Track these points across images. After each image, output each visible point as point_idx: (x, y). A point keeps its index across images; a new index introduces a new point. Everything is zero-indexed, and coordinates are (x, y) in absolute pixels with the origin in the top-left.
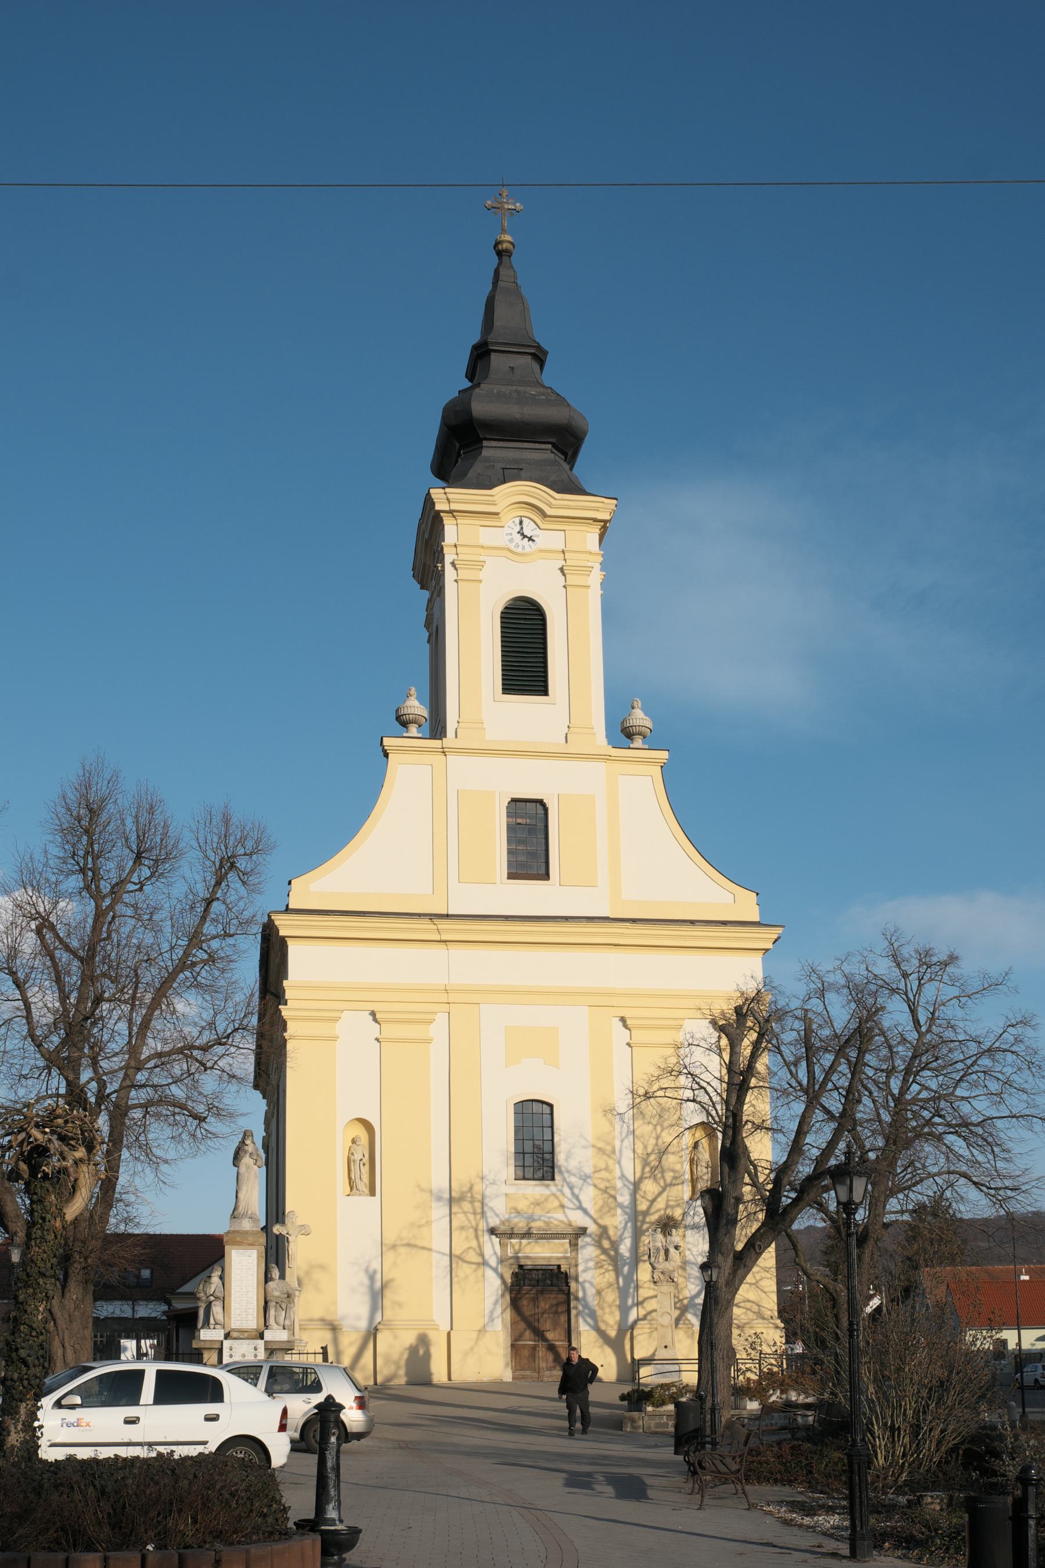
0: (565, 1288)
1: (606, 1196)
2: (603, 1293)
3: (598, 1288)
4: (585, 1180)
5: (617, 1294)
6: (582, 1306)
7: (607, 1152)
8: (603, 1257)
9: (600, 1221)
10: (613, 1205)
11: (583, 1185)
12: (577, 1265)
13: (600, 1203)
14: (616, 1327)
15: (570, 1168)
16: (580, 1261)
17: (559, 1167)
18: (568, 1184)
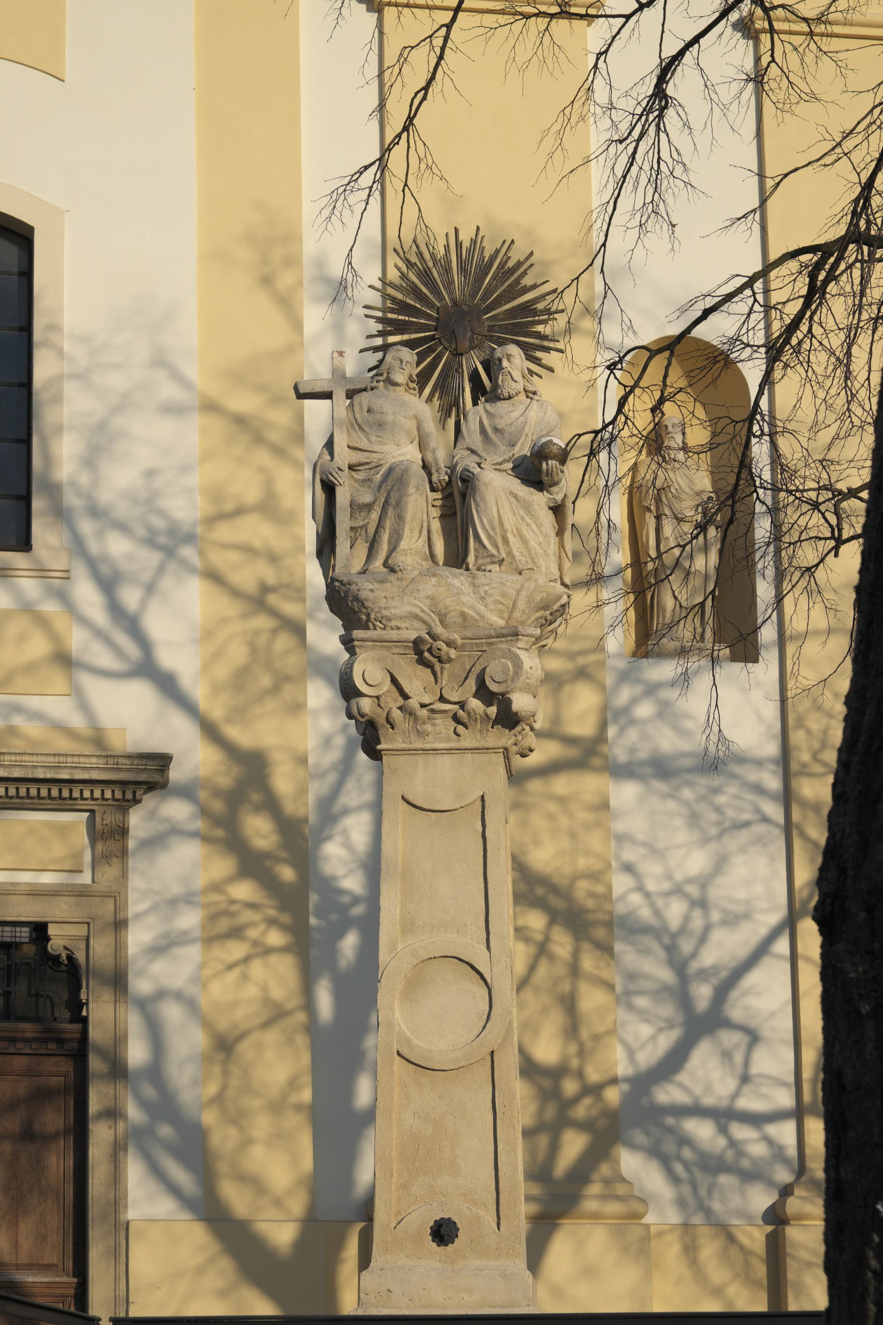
0: (71, 1029)
1: (263, 622)
2: (245, 1047)
3: (223, 1024)
4: (169, 552)
5: (306, 1058)
6: (144, 1104)
7: (273, 436)
8: (244, 891)
9: (234, 733)
10: (293, 663)
11: (161, 570)
12: (120, 925)
13: (238, 653)
14: (298, 1205)
15: (105, 496)
16: (135, 905)
17: (54, 490)
18: (93, 565)
